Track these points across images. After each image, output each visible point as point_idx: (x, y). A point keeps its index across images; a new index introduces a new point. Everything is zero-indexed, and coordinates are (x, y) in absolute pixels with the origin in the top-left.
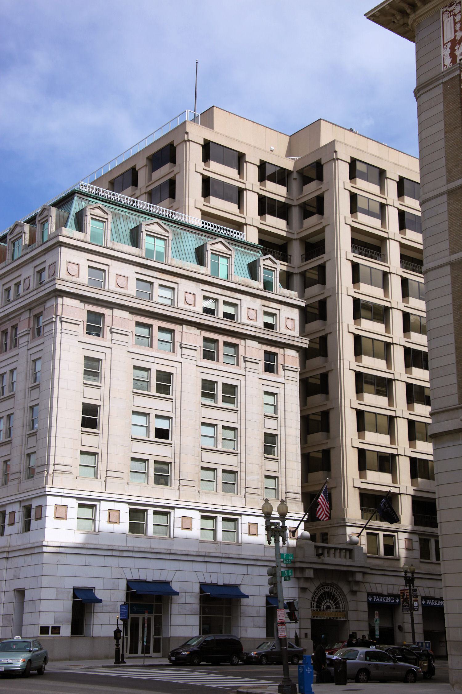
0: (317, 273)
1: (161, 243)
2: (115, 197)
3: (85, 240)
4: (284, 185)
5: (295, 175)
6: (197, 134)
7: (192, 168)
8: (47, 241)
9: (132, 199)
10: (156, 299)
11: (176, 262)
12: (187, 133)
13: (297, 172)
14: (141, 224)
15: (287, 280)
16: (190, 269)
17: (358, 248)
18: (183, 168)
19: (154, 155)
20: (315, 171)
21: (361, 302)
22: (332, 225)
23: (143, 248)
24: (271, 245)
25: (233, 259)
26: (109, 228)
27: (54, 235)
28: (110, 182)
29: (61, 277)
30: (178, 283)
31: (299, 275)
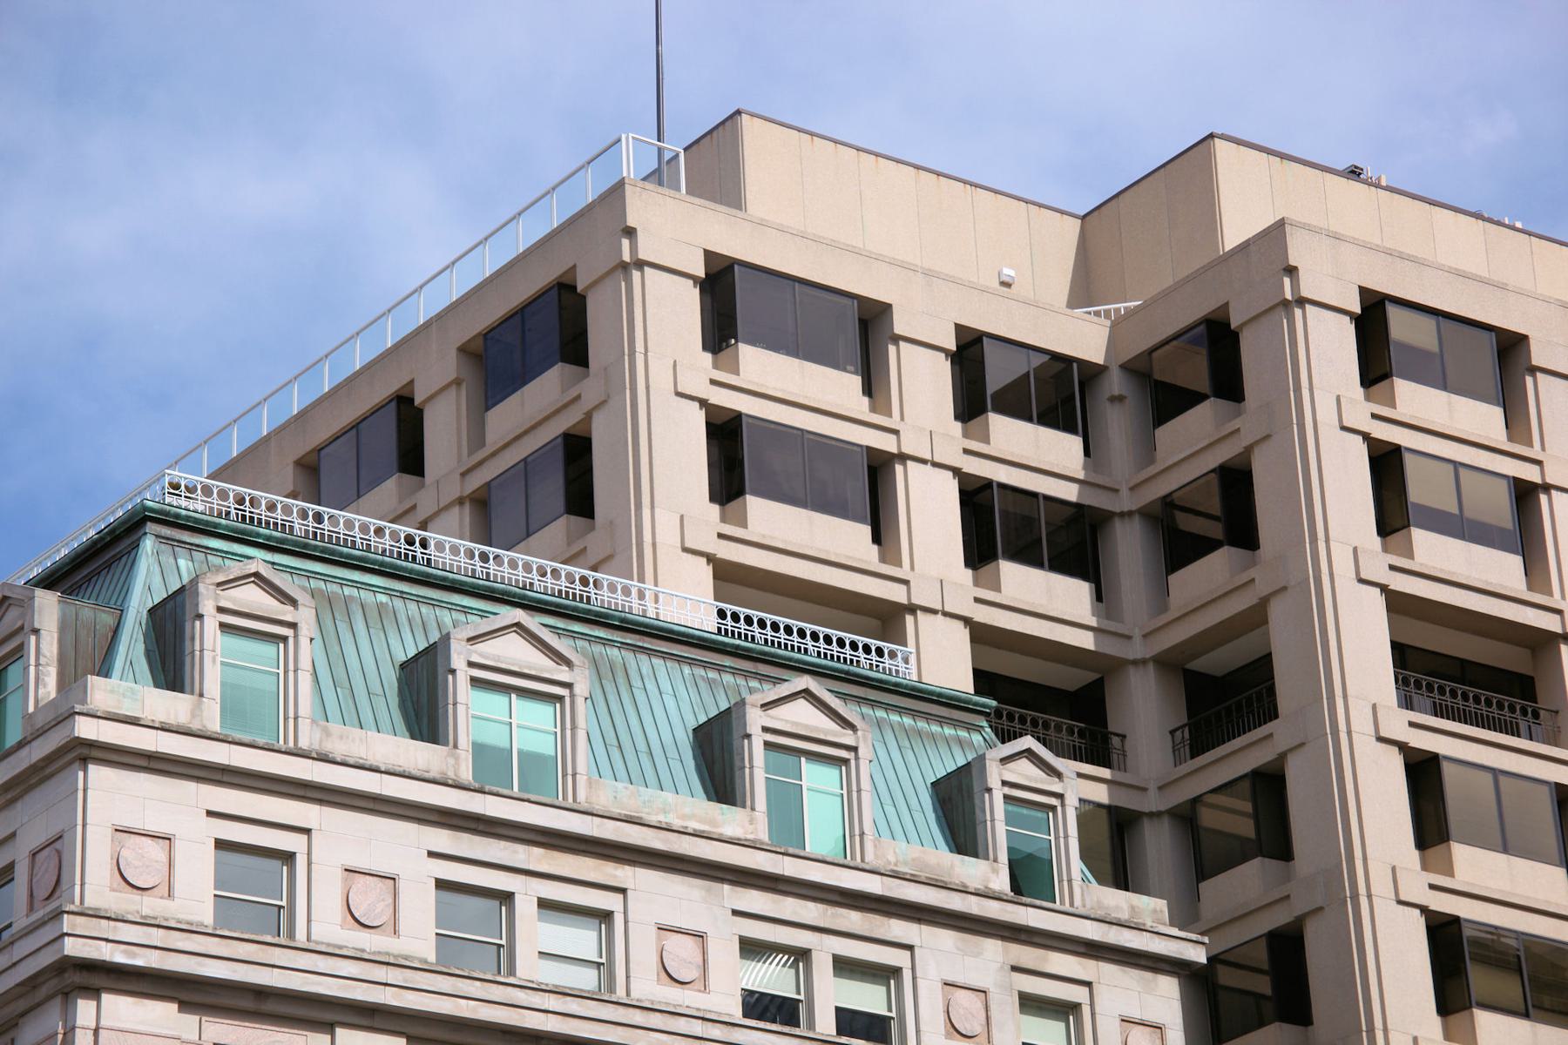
0: (1248, 807)
1: (542, 714)
2: (326, 525)
3: (195, 726)
4: (1070, 428)
5: (1115, 383)
6: (676, 230)
7: (661, 380)
8: (21, 745)
9: (404, 530)
10: (528, 967)
11: (613, 794)
12: (630, 232)
13: (1126, 367)
14: (446, 638)
15: (1116, 848)
16: (677, 823)
17: (1430, 687)
18: (619, 385)
19: (488, 335)
20: (1207, 360)
21: (1467, 932)
22: (1301, 589)
23: (463, 741)
24: (1031, 695)
25: (864, 764)
26: (305, 663)
27: (51, 716)
28: (300, 464)
29: (90, 902)
30: (623, 891)
31: (1137, 518)
